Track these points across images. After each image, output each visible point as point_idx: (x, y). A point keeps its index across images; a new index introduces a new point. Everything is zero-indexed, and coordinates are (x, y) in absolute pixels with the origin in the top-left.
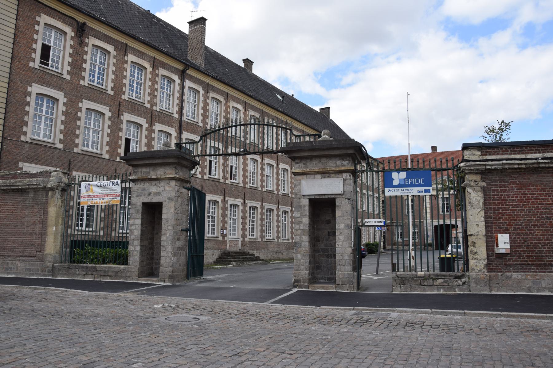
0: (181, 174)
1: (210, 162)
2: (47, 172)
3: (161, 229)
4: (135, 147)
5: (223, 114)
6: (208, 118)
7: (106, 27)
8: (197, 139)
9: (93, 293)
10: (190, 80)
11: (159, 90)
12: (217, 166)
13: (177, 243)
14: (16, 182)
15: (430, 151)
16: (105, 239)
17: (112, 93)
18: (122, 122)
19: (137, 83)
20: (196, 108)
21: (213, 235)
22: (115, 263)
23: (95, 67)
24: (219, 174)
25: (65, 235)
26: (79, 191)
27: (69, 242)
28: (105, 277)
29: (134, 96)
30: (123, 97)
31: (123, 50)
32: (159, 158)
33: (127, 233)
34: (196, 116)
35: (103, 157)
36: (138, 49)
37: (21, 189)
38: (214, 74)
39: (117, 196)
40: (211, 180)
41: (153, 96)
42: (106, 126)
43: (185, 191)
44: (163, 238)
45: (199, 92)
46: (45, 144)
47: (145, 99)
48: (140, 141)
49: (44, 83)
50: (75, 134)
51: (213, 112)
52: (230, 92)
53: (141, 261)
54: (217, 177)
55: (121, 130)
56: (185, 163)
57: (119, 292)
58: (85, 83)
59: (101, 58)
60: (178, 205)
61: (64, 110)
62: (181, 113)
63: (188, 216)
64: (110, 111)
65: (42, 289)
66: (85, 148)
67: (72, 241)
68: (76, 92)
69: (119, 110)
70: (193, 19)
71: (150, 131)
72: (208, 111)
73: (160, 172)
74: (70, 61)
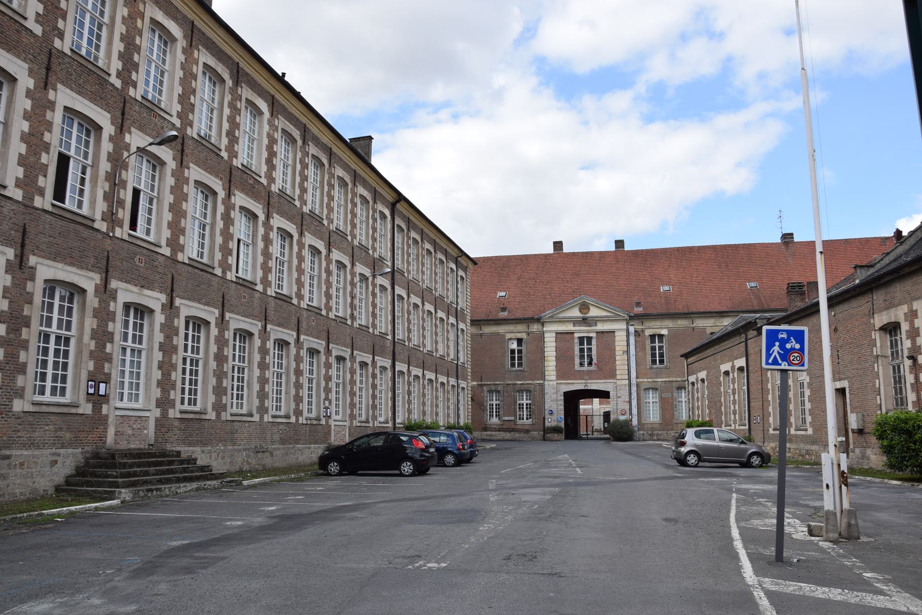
5: (120, 28)
21: (58, 399)
24: (93, 203)
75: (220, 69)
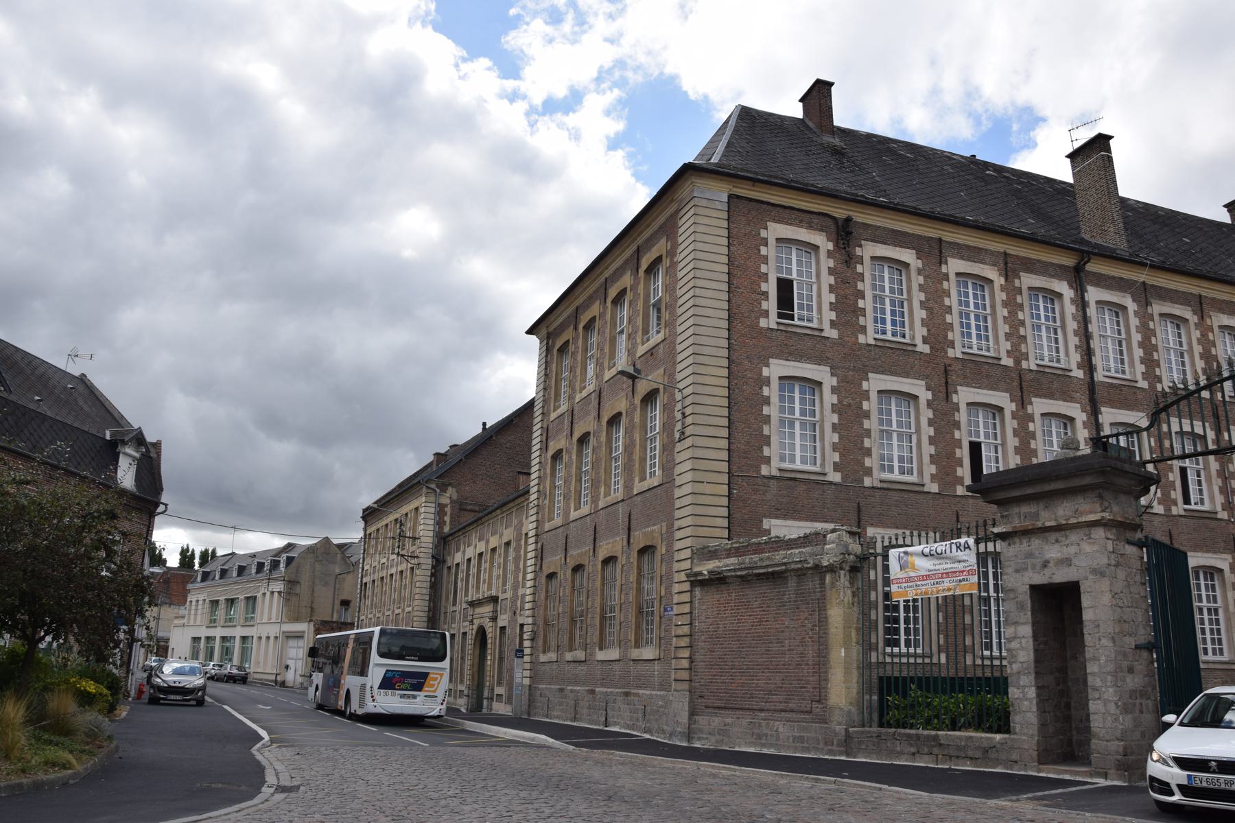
0: (1117, 510)
1: (1183, 471)
2: (817, 534)
3: (1084, 646)
4: (993, 459)
5: (1198, 349)
6: (1159, 366)
7: (891, 214)
8: (1144, 423)
9: (939, 797)
10: (1097, 285)
11: (1028, 323)
12: (1203, 478)
13: (1128, 680)
14: (761, 560)
15: (620, 154)
16: (952, 673)
17: (926, 349)
18: (956, 408)
19: (977, 318)
20: (1124, 348)
21: (1218, 658)
22: (979, 727)
23: (883, 303)
24: (1212, 498)
25: (865, 666)
26: (886, 569)
27: (875, 680)
28: (961, 761)
29: (975, 347)
30: (950, 353)
31: (935, 252)
32: (1058, 478)
33: (1001, 658)
34: (1126, 366)
35: (926, 489)
36: (966, 243)
37: (773, 573)
38: (1155, 258)
39: (970, 573)
40: (1191, 515)
41: (1016, 338)
42: (924, 422)
43: (1131, 550)
44: (1092, 668)
45: (1125, 308)
46: (806, 476)
47: (1001, 350)
48: (1004, 444)
49: (790, 354)
50: (862, 448)
51: (1168, 349)
52: (1204, 293)
53: (1043, 725)
54: (1207, 507)
55: (957, 425)
56: (1121, 481)
57: (997, 797)
58: (868, 338)
59: (891, 281)
60: (1120, 585)
61: (835, 401)
62: (1089, 367)
63: (1147, 611)
64: (928, 389)
65: (830, 783)
66: (886, 476)
67: (881, 679)
68: (853, 361)
69: (947, 383)
70: (1077, 145)
71: (1023, 417)
72: (1155, 348)
73: (1063, 511)
74: (833, 300)
75: (1177, 310)
